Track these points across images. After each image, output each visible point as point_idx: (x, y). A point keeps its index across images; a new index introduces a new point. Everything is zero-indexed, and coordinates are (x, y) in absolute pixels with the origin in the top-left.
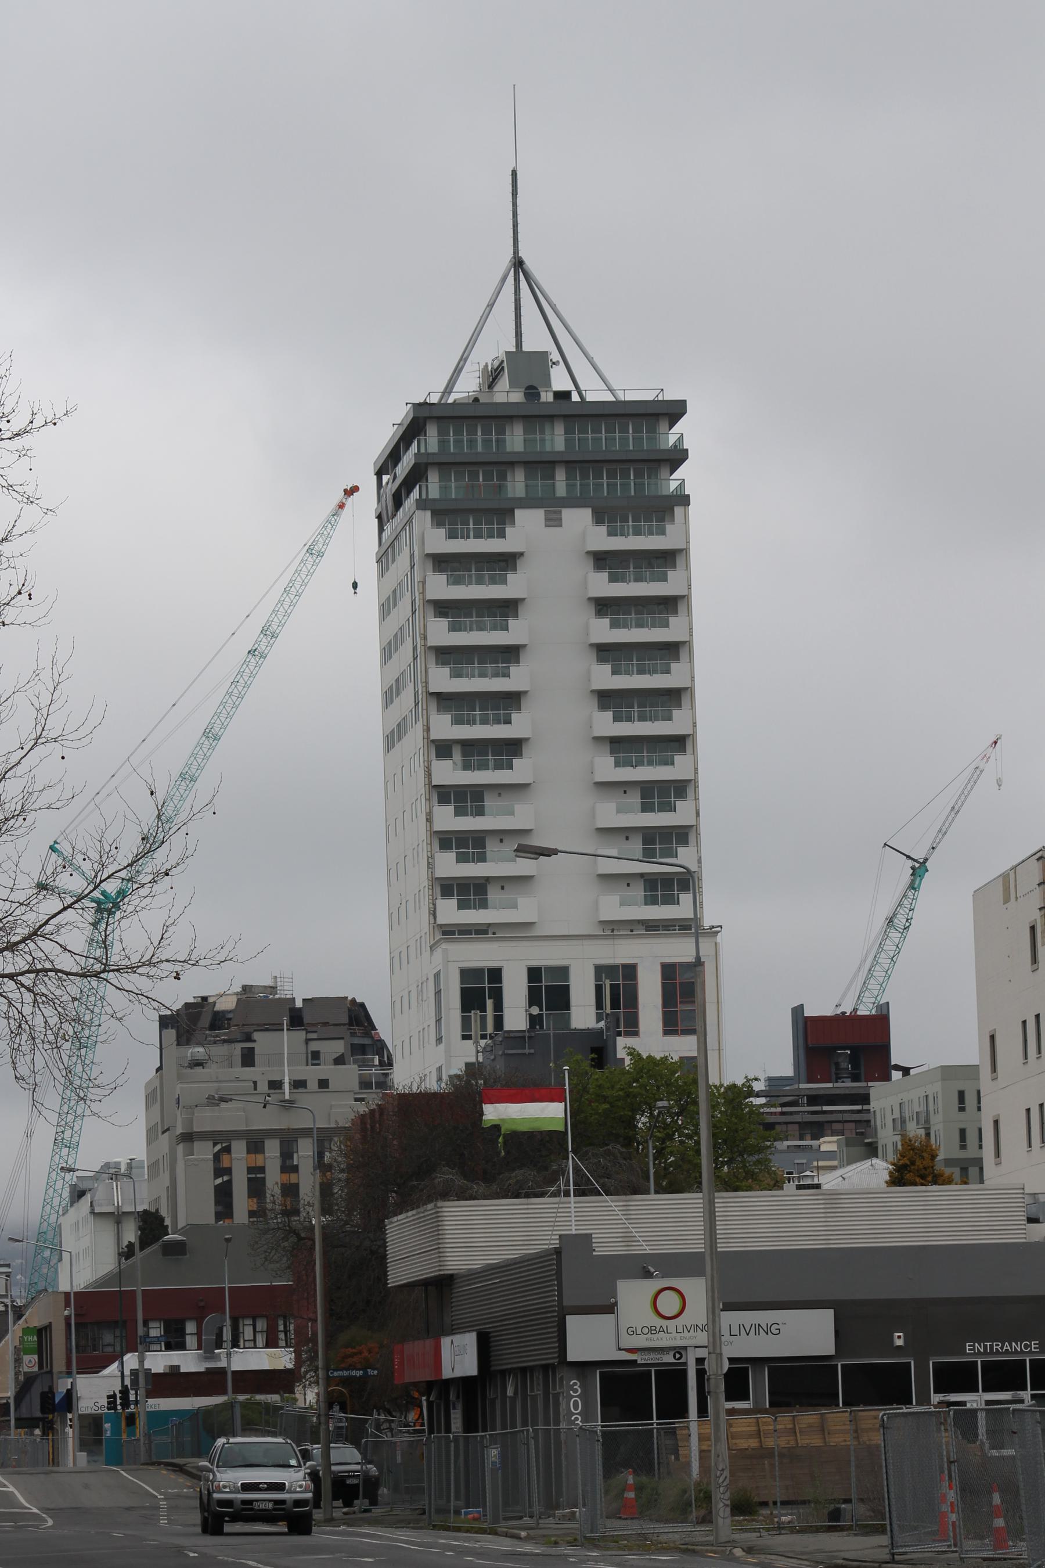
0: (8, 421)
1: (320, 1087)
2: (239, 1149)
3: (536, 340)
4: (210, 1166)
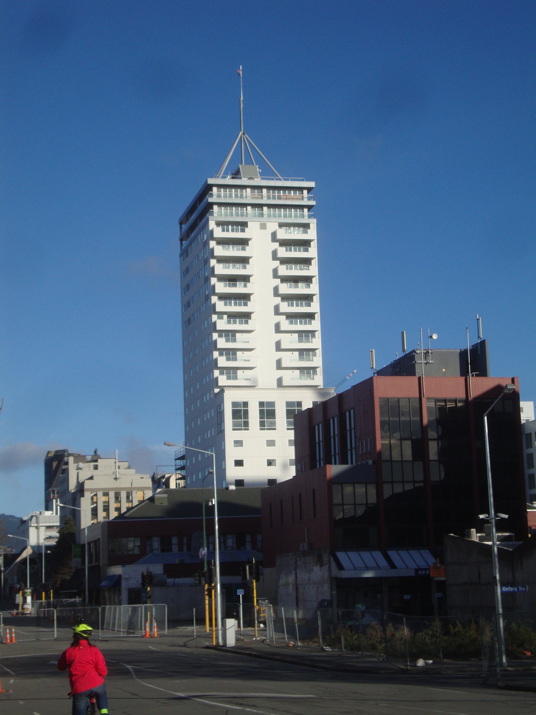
0: (270, 463)
2: (100, 494)
4: (90, 500)
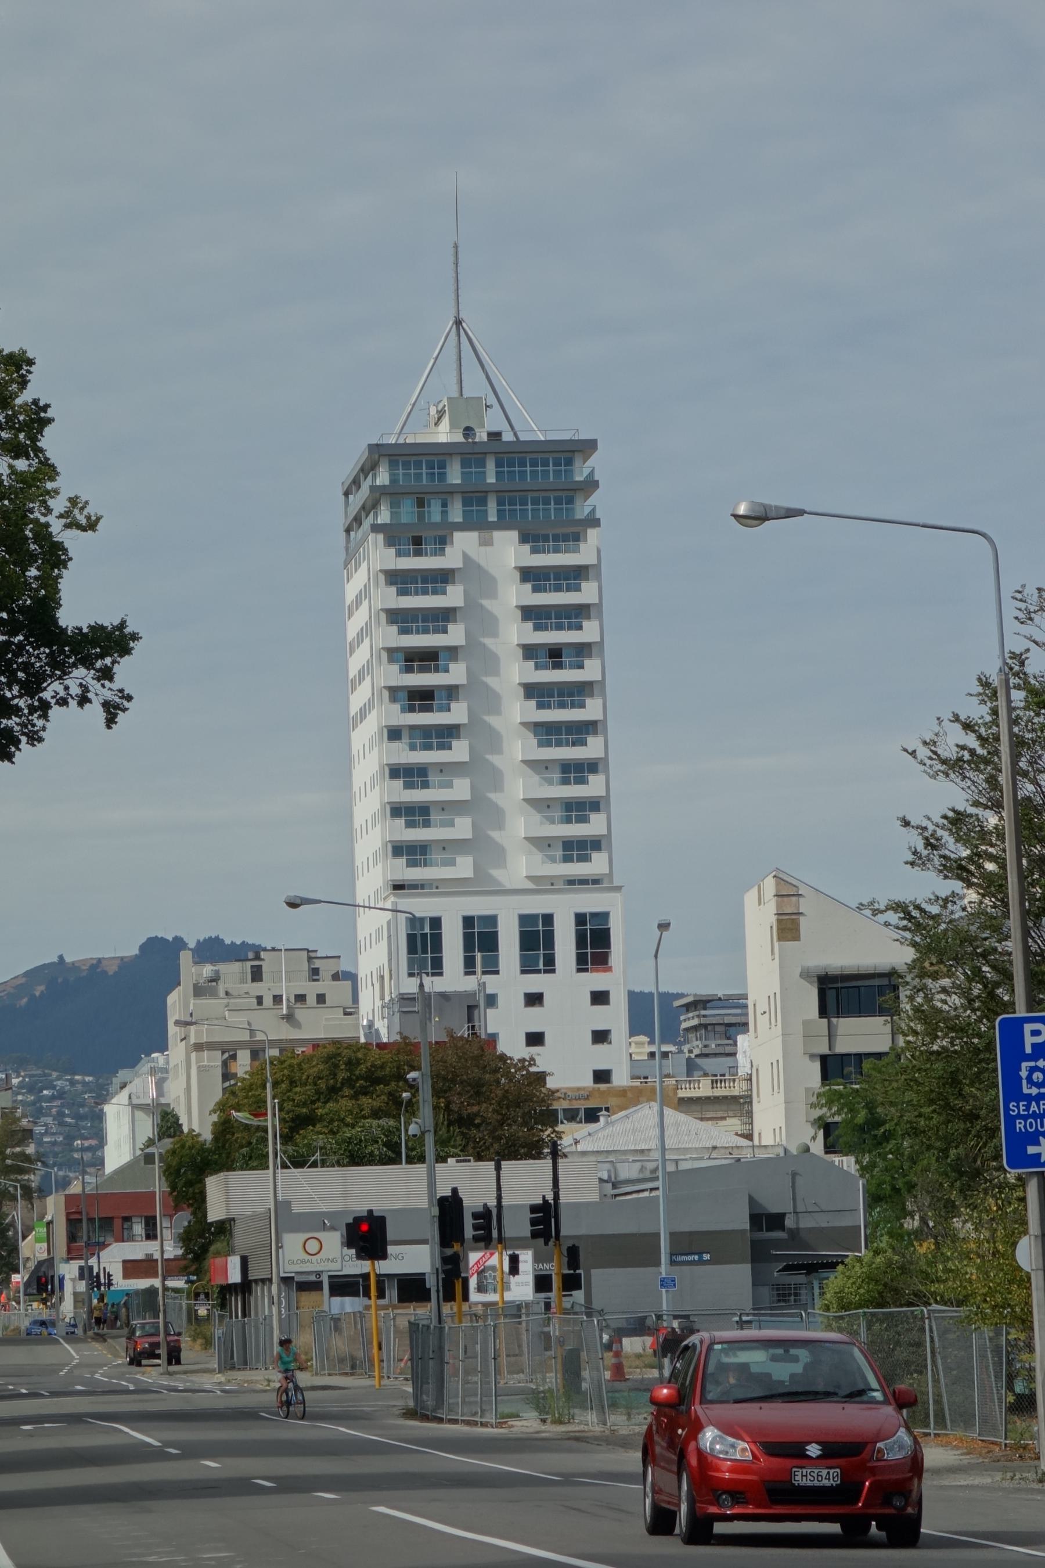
1: (318, 1003)
3: (475, 386)
4: (219, 1072)
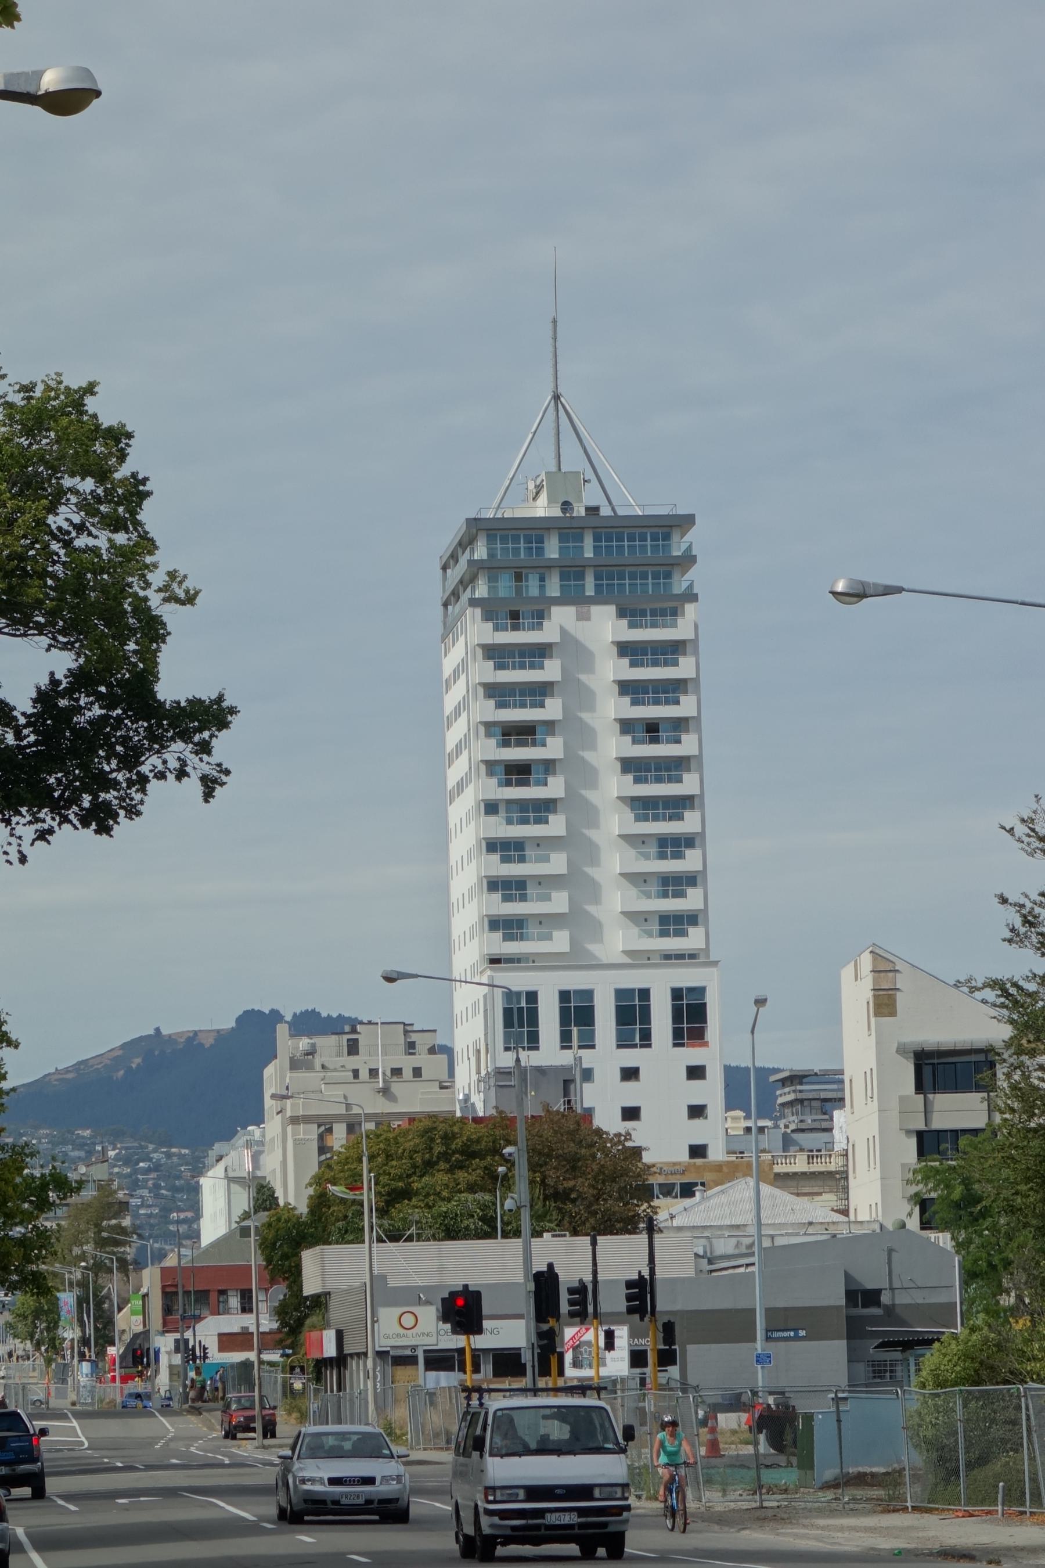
3: (573, 461)
